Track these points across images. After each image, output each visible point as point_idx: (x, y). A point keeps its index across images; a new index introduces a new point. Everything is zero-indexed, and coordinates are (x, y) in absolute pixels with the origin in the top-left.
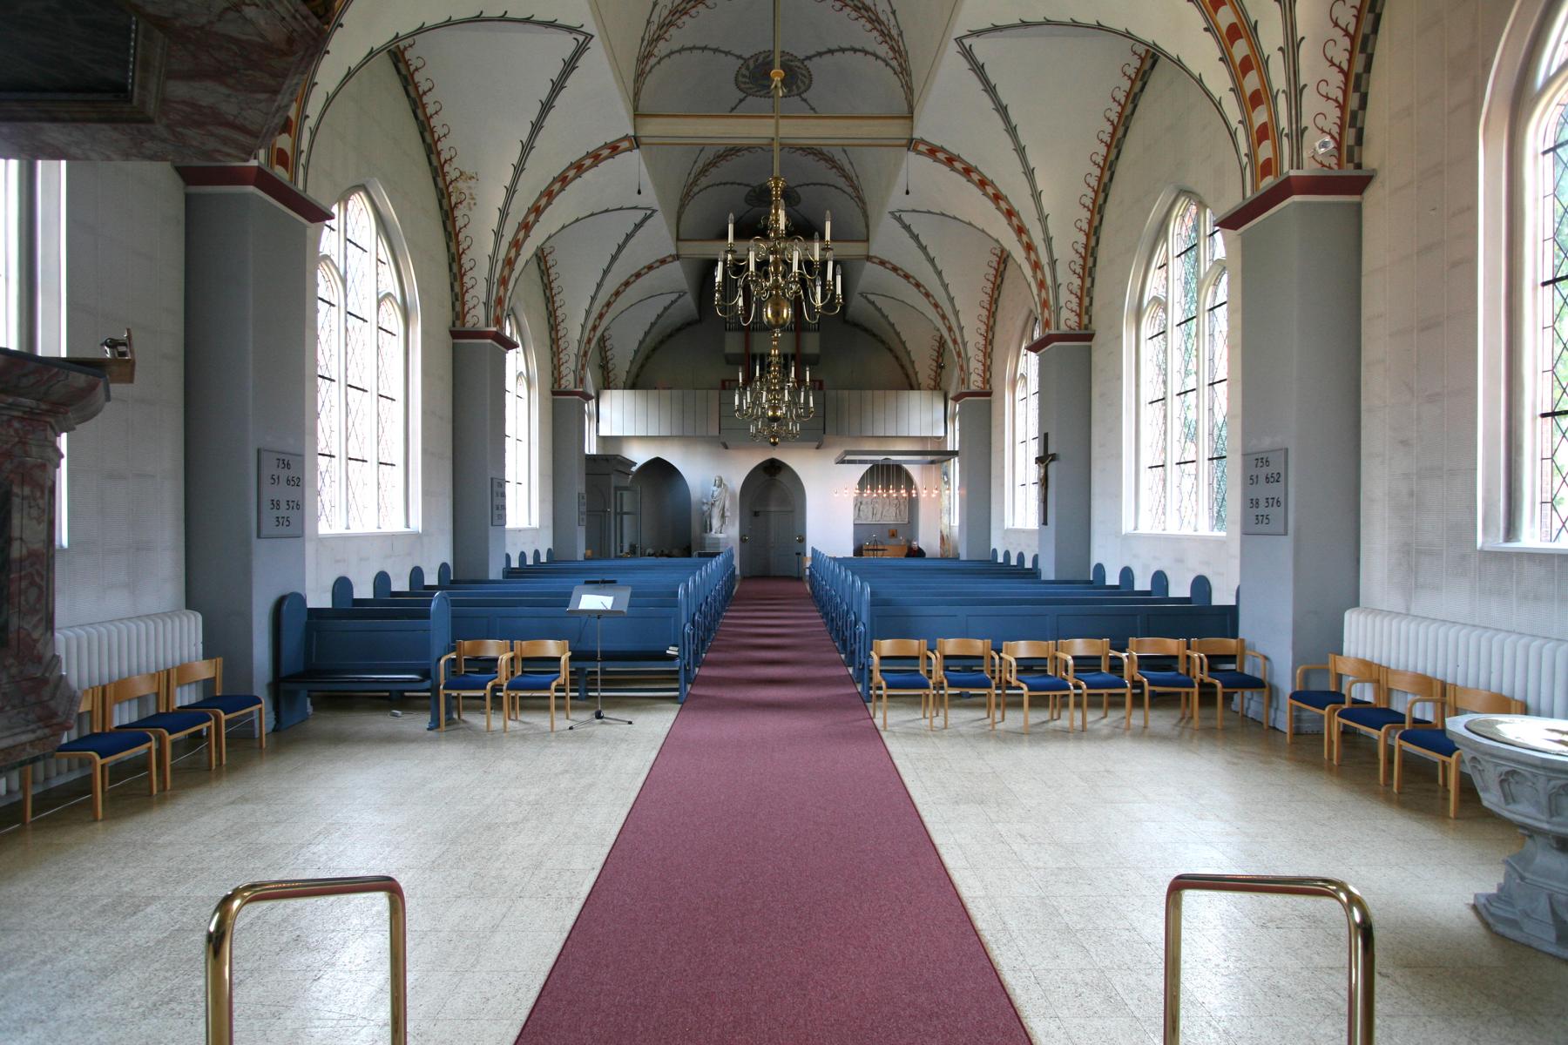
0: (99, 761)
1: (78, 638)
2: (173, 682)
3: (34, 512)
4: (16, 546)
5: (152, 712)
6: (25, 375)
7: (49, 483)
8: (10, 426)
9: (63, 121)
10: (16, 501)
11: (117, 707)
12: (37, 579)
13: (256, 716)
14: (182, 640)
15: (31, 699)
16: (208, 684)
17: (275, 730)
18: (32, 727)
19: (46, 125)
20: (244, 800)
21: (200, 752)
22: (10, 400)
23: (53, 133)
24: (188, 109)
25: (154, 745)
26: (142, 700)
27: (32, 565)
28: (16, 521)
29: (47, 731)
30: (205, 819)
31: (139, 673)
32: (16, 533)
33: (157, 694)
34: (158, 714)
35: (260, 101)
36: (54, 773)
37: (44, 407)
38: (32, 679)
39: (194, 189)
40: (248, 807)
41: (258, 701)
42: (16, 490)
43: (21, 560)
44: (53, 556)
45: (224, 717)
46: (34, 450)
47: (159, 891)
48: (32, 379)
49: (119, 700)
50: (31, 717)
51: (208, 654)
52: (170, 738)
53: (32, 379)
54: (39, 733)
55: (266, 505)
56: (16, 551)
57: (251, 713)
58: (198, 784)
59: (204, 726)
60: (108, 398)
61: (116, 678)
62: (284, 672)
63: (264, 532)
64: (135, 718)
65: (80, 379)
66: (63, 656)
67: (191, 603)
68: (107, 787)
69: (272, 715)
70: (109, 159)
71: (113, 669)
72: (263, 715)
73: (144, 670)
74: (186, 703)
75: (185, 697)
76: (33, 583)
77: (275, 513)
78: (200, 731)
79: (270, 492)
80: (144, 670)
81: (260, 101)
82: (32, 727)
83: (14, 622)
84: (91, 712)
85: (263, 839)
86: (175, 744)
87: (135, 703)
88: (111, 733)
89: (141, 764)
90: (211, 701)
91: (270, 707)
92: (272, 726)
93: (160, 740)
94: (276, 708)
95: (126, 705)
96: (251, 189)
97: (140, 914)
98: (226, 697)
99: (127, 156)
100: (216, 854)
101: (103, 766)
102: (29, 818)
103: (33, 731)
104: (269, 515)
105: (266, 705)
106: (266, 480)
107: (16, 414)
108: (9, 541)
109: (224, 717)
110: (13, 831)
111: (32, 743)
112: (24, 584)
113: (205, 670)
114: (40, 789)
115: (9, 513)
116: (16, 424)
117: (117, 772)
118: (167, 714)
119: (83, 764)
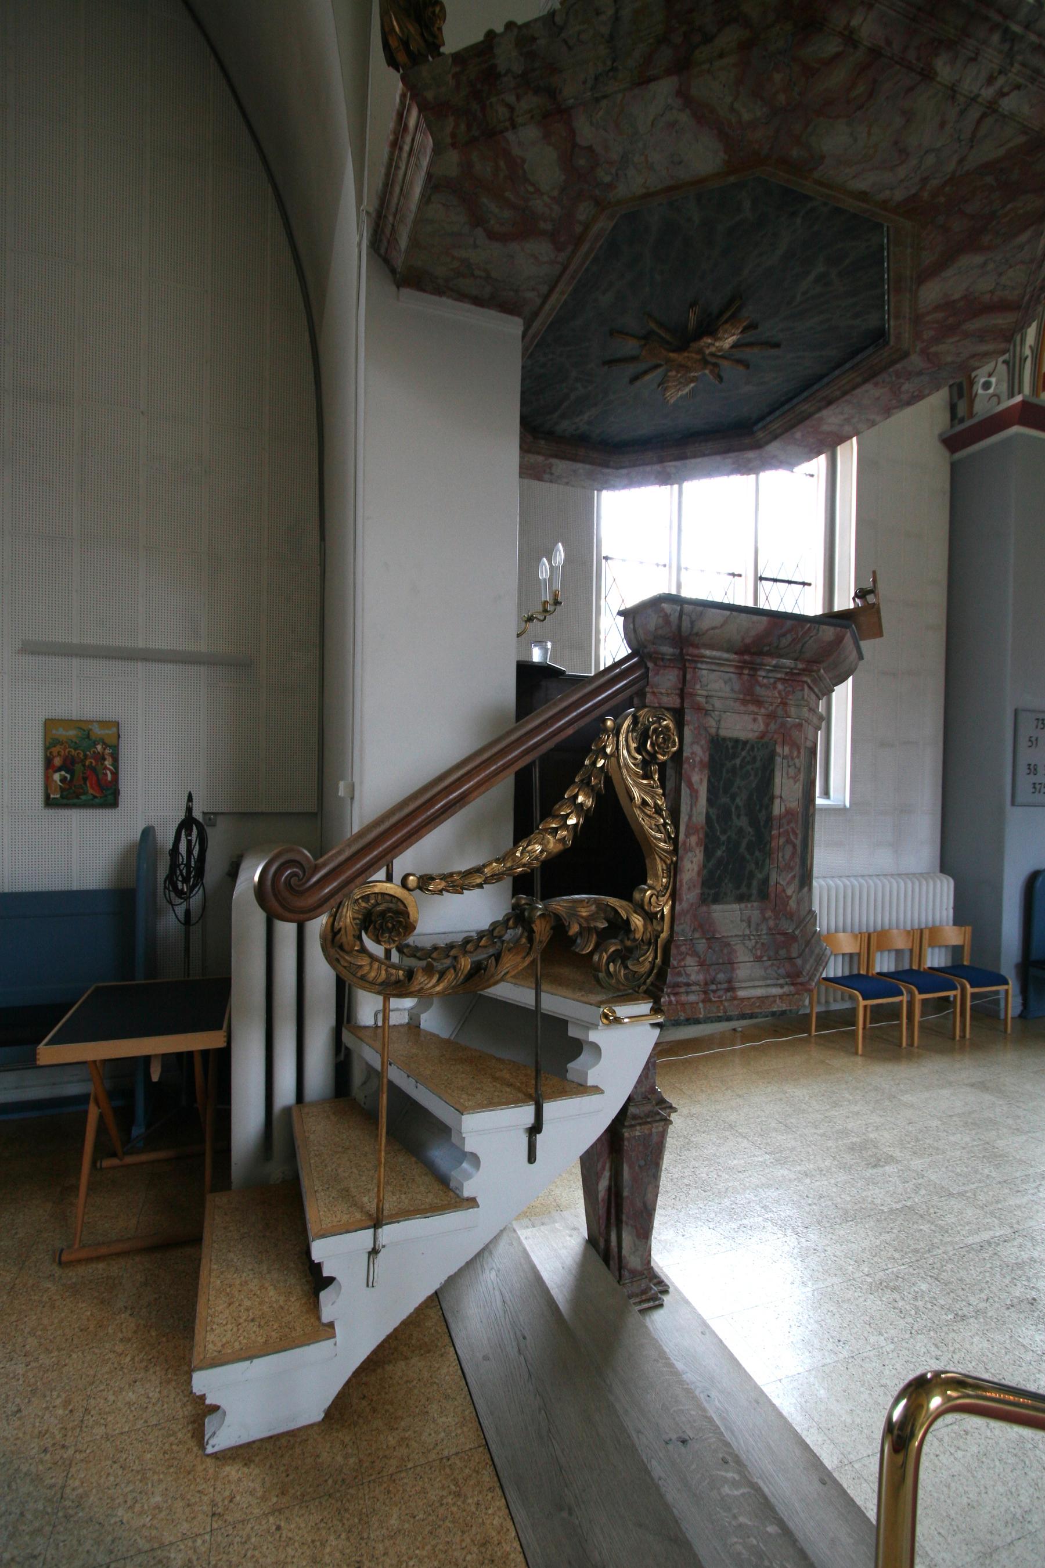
0: (862, 1003)
1: (861, 885)
2: (925, 942)
3: (792, 771)
4: (777, 801)
5: (907, 967)
6: (784, 635)
7: (809, 744)
8: (775, 688)
9: (837, 399)
10: (778, 760)
11: (878, 955)
12: (792, 837)
13: (1002, 996)
14: (934, 902)
15: (783, 953)
16: (956, 951)
17: (1020, 1016)
18: (781, 981)
19: (825, 413)
20: (983, 1086)
21: (945, 1017)
22: (774, 662)
23: (831, 418)
24: (940, 315)
25: (905, 998)
26: (899, 953)
27: (789, 823)
28: (777, 780)
29: (792, 988)
30: (945, 1092)
31: (897, 927)
32: (777, 792)
33: (911, 951)
34: (911, 970)
35: (1021, 247)
36: (831, 1000)
37: (800, 666)
38: (785, 934)
39: (959, 455)
40: (987, 1097)
41: (1006, 983)
42: (779, 750)
43: (780, 817)
44: (813, 815)
45: (970, 990)
46: (793, 710)
47: (897, 1154)
48: (789, 638)
49: (881, 948)
50: (782, 971)
51: (959, 919)
52: (919, 997)
53: (789, 638)
54: (786, 989)
55: (1022, 769)
56: (777, 809)
57: (997, 992)
58: (942, 1051)
59: (951, 993)
60: (861, 657)
61: (879, 928)
62: (1035, 956)
63: (1019, 799)
64: (892, 969)
65: (828, 633)
66: (817, 912)
67: (945, 866)
68: (868, 1026)
69: (1019, 1000)
70: (873, 424)
71: (871, 919)
72: (1010, 996)
73: (901, 927)
74: (936, 965)
75: (935, 959)
76: (788, 841)
77: (1032, 779)
78: (948, 997)
79: (1027, 756)
80: (901, 927)
81: (1021, 247)
82: (781, 981)
83: (773, 878)
84: (859, 954)
85: (1000, 1143)
86: (924, 1002)
87: (893, 954)
88: (873, 978)
89: (893, 1012)
90: (958, 969)
91: (1018, 990)
92: (1019, 1010)
93: (911, 993)
94: (1024, 991)
95: (886, 954)
96: (1016, 429)
97: (880, 1170)
98: (971, 969)
99: (888, 412)
100: (952, 1138)
101: (865, 1007)
102: (814, 1033)
103: (782, 986)
104: (1025, 782)
105: (1012, 987)
106: (1023, 742)
107: (779, 676)
108: (772, 798)
109: (970, 990)
110: (801, 1039)
111: (781, 997)
112: (782, 841)
113: (954, 936)
114: (823, 1009)
115: (773, 771)
116: (780, 686)
117: (877, 1014)
118: (918, 972)
119: (852, 998)
